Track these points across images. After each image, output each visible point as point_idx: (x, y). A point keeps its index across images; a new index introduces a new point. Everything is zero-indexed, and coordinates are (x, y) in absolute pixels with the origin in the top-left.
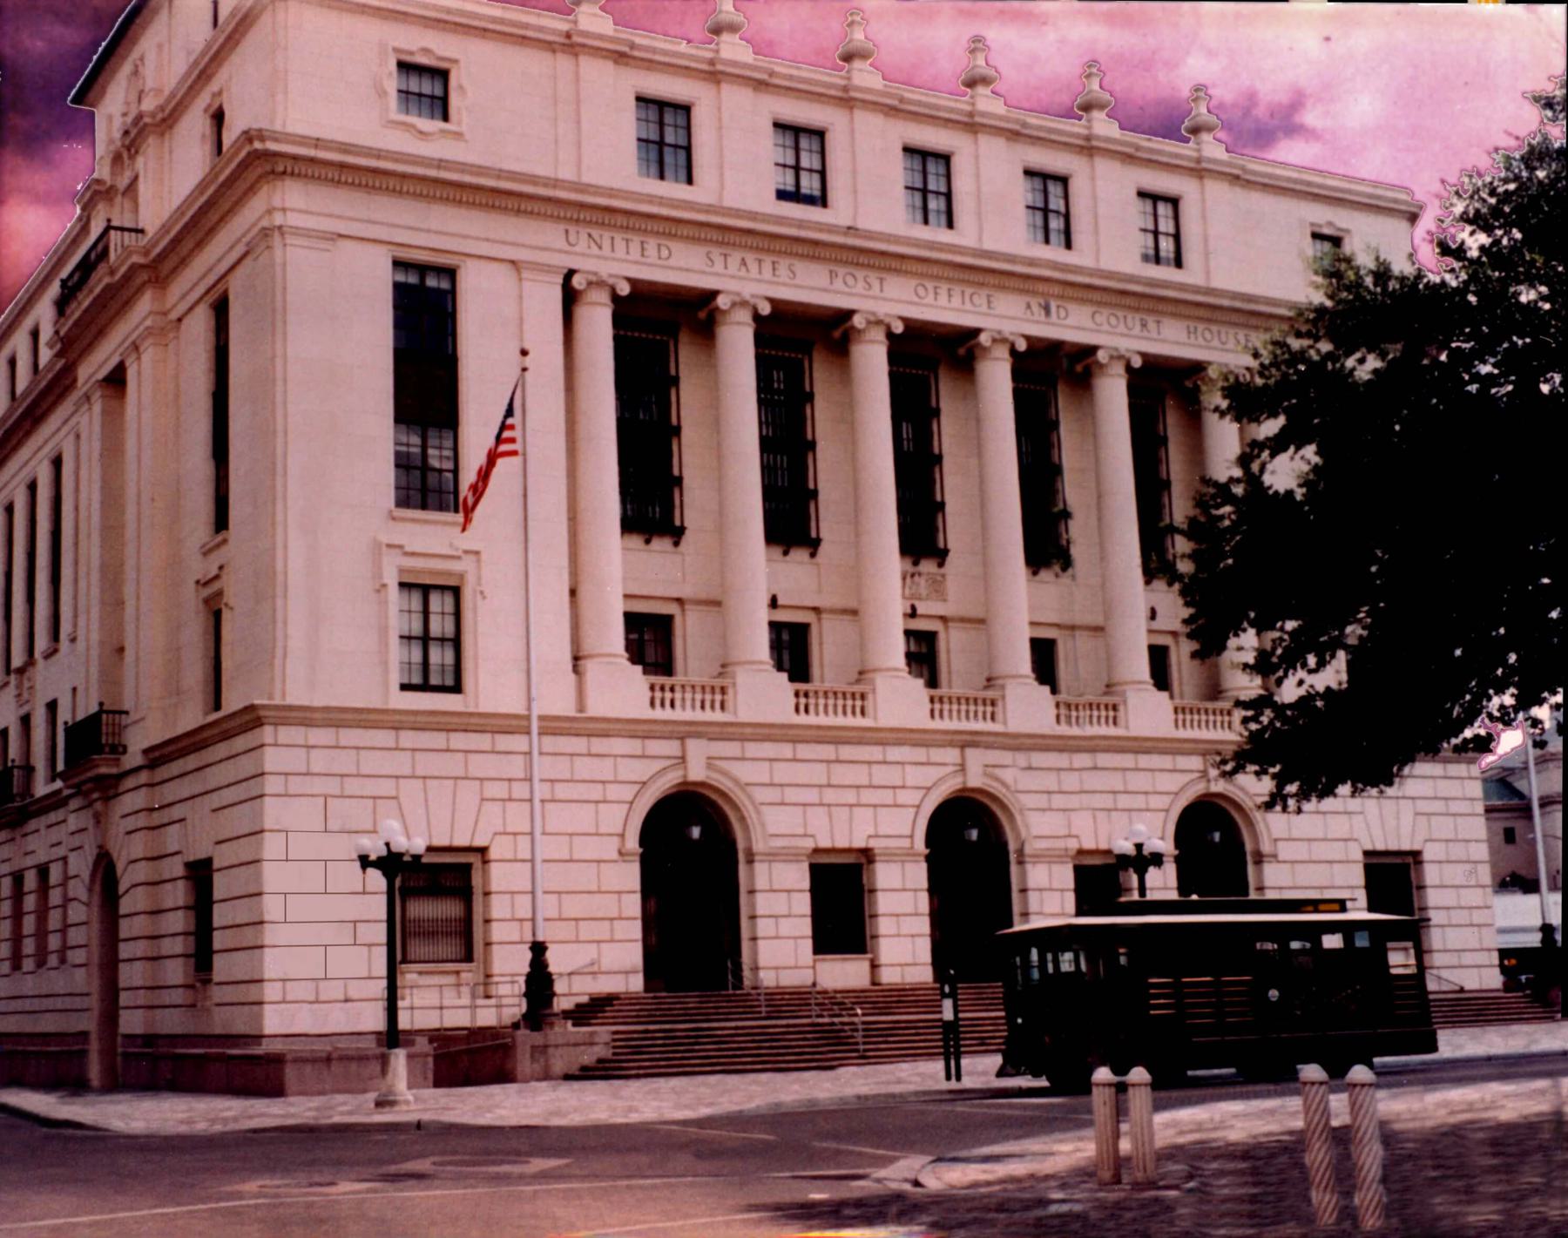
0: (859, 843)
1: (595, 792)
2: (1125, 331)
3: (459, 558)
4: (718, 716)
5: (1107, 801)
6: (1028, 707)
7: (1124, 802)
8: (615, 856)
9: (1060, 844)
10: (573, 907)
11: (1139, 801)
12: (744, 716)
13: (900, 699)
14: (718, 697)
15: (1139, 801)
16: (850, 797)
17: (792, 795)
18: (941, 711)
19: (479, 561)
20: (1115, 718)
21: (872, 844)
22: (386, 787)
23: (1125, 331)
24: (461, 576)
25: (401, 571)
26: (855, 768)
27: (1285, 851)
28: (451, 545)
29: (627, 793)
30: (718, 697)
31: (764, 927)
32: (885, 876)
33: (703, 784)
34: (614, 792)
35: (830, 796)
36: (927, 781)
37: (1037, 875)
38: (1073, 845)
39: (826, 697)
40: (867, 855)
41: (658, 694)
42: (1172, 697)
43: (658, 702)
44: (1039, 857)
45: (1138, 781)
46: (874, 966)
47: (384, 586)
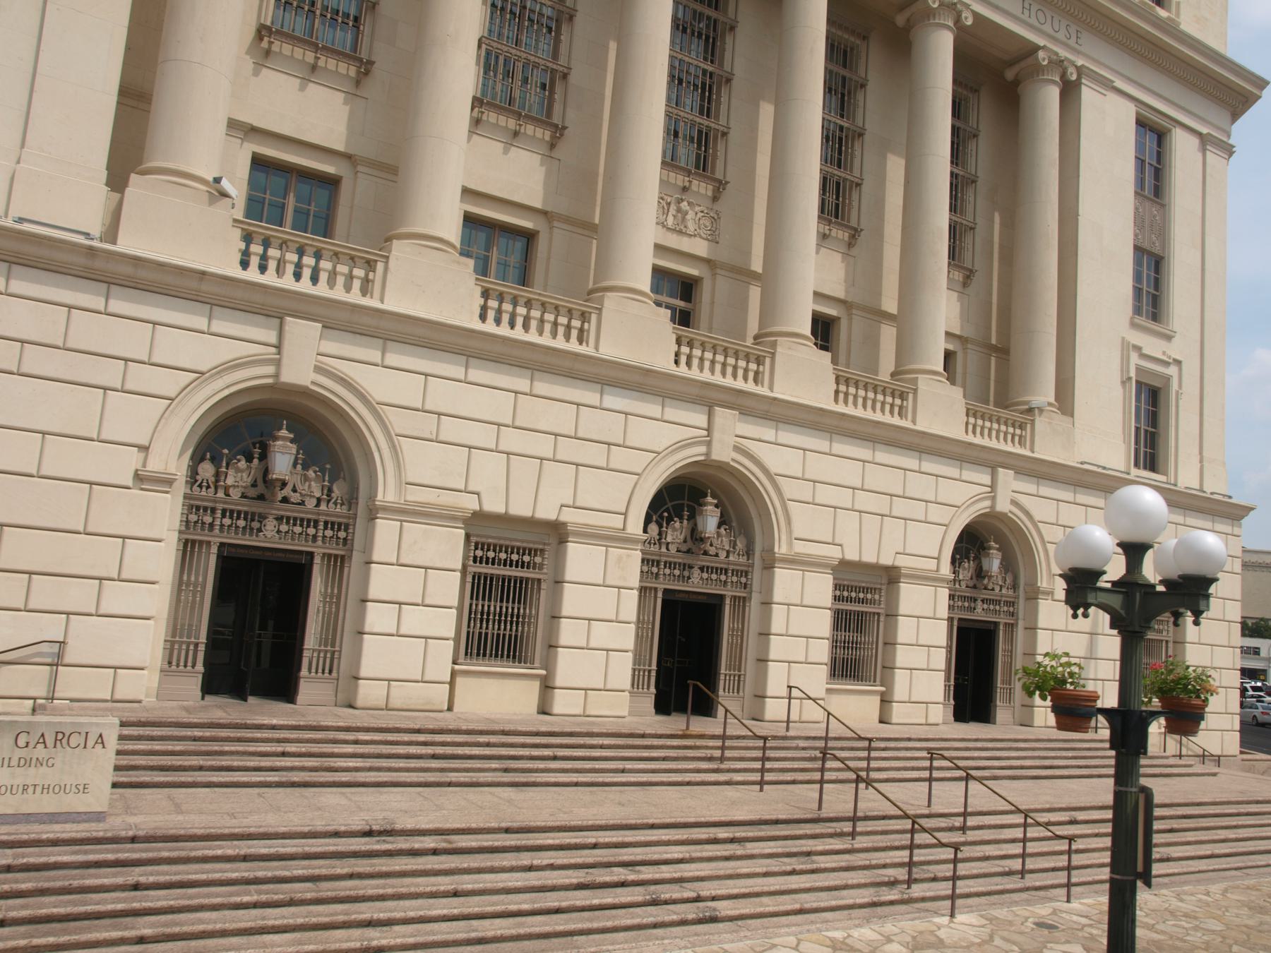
0: (547, 512)
1: (110, 373)
2: (1050, 31)
3: (1166, 364)
5: (881, 504)
6: (803, 376)
7: (568, 449)
8: (130, 484)
9: (447, 499)
11: (918, 510)
12: (609, 350)
13: (635, 331)
14: (576, 323)
15: (918, 510)
16: (543, 446)
17: (451, 429)
18: (689, 357)
19: (1180, 370)
20: (757, 373)
21: (568, 516)
23: (1050, 31)
24: (1168, 379)
25: (1139, 369)
26: (554, 407)
28: (1164, 353)
31: (157, 601)
32: (581, 560)
33: (304, 392)
34: (936, 513)
35: (512, 440)
36: (662, 441)
37: (785, 582)
38: (471, 504)
39: (515, 304)
40: (558, 533)
41: (493, 304)
42: (835, 361)
43: (683, 359)
44: (795, 562)
45: (920, 486)
46: (886, 701)
47: (1130, 379)
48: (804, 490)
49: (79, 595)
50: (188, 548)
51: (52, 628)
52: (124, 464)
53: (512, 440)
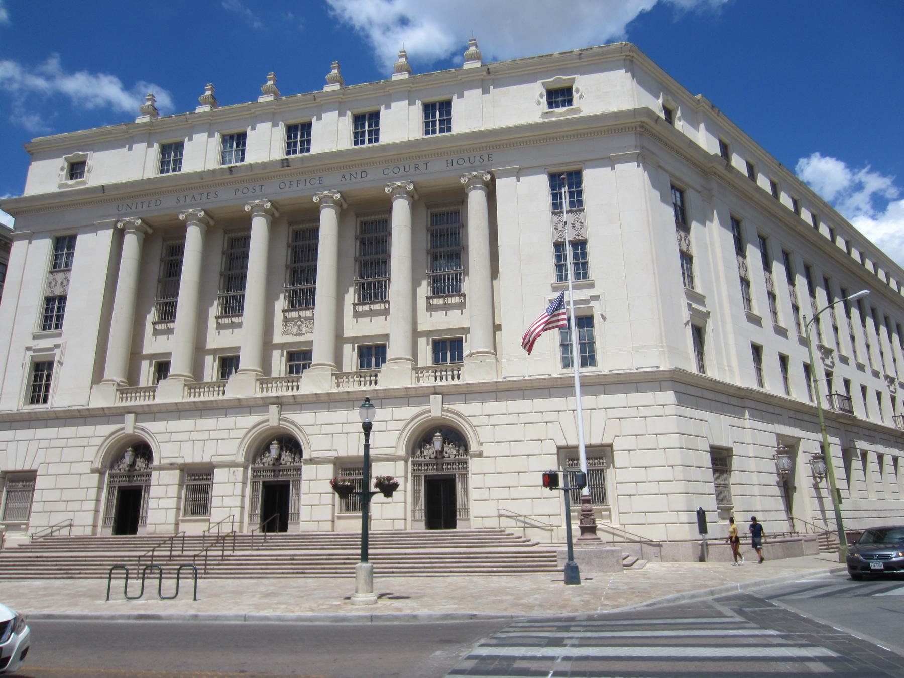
0: (206, 459)
1: (84, 442)
4: (456, 382)
10: (490, 480)
11: (224, 434)
17: (325, 429)
22: (553, 416)
27: (487, 450)
29: (99, 441)
30: (455, 372)
35: (195, 436)
37: (307, 471)
38: (335, 454)
48: (316, 430)
49: (75, 506)
50: (416, 477)
51: (70, 515)
52: (86, 467)
53: (195, 436)
